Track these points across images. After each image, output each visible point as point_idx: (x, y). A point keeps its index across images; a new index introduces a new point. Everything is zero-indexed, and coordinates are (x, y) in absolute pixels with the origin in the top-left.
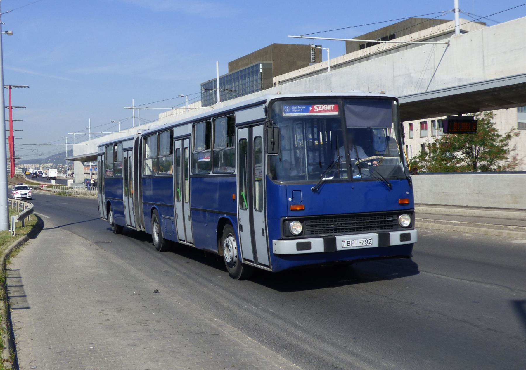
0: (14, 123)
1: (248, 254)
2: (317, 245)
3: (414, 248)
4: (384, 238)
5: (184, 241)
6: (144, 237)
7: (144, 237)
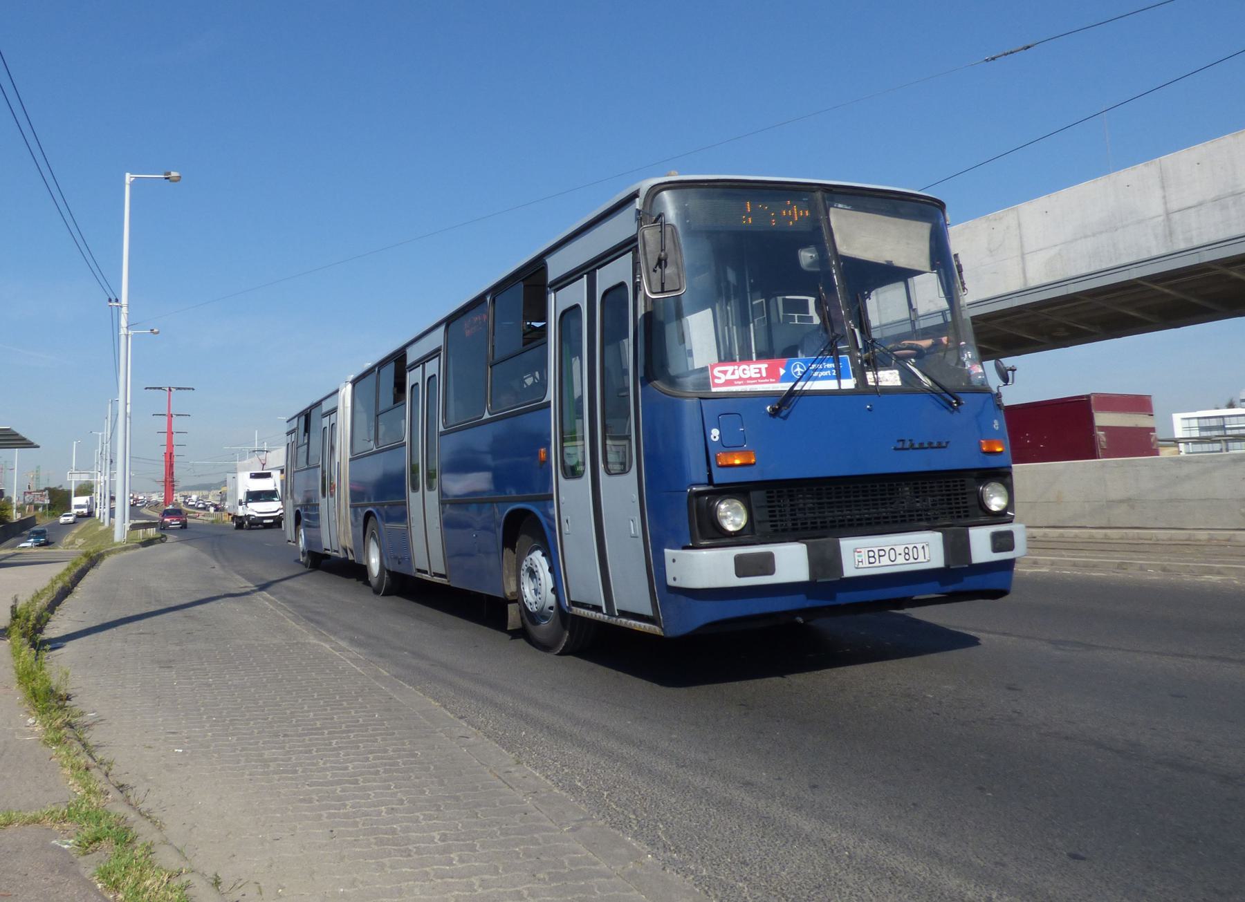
0: (175, 419)
1: (585, 586)
2: (791, 562)
3: (1018, 568)
4: (957, 547)
5: (426, 572)
6: (354, 571)
7: (354, 571)
